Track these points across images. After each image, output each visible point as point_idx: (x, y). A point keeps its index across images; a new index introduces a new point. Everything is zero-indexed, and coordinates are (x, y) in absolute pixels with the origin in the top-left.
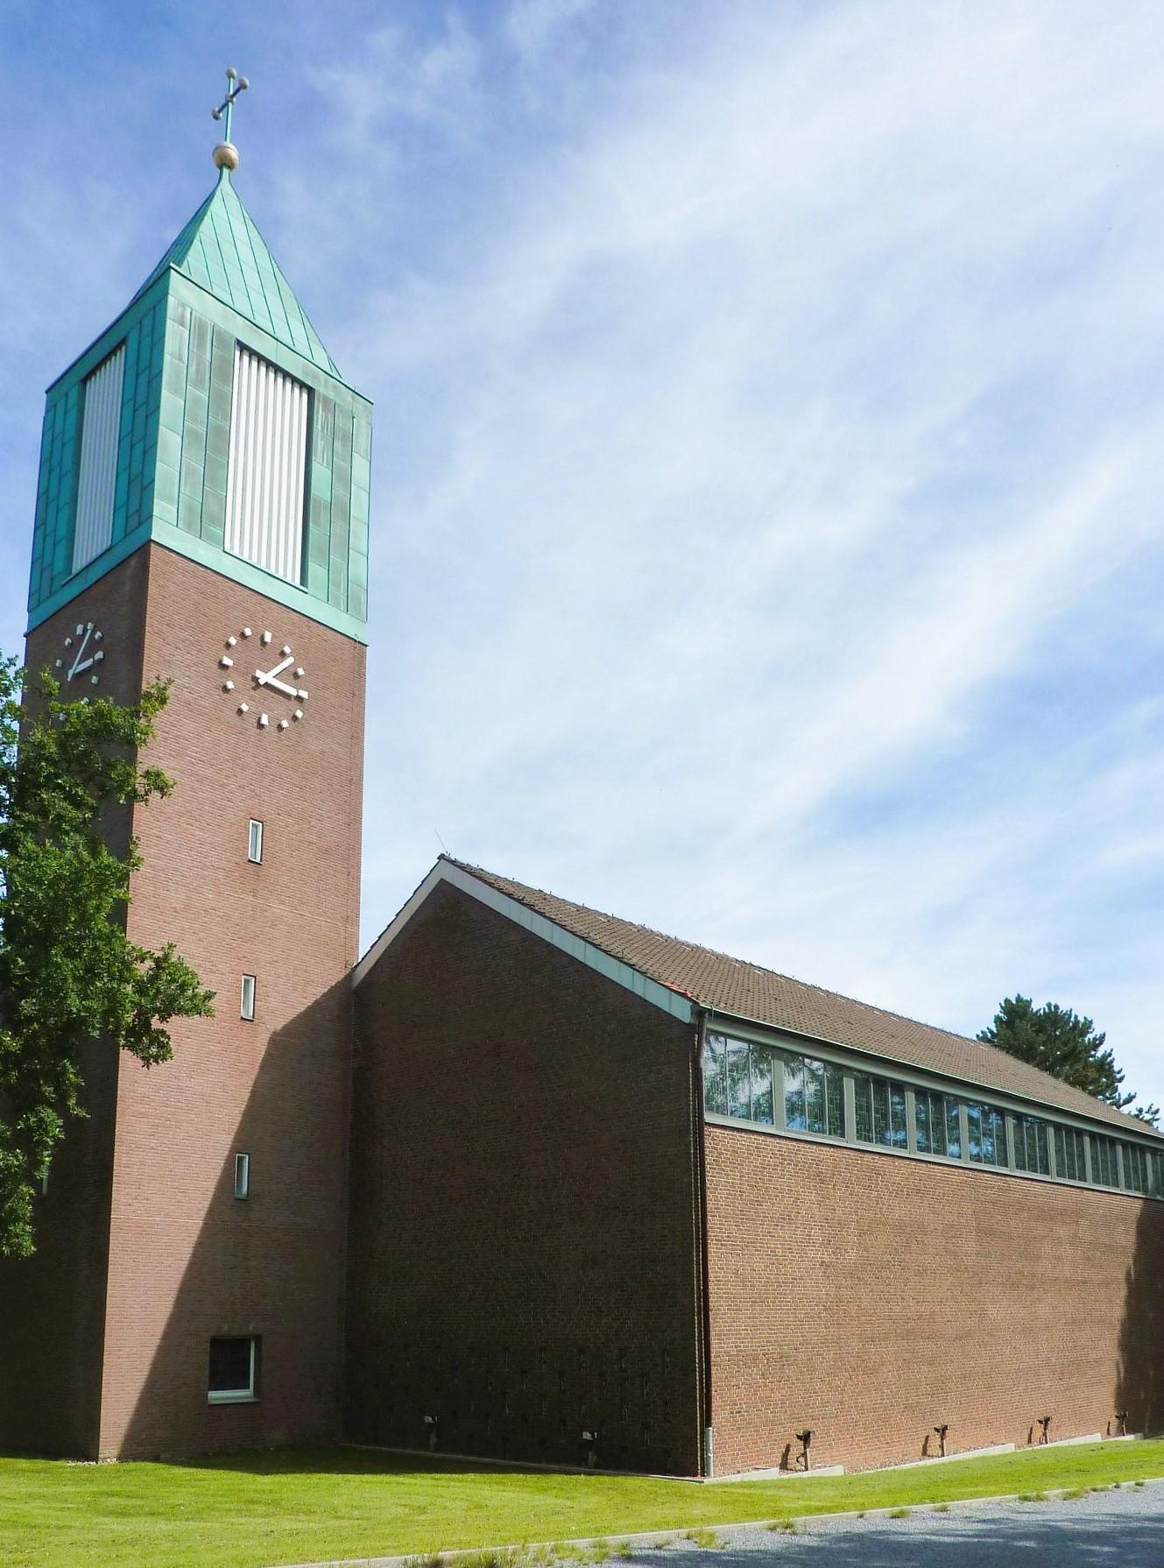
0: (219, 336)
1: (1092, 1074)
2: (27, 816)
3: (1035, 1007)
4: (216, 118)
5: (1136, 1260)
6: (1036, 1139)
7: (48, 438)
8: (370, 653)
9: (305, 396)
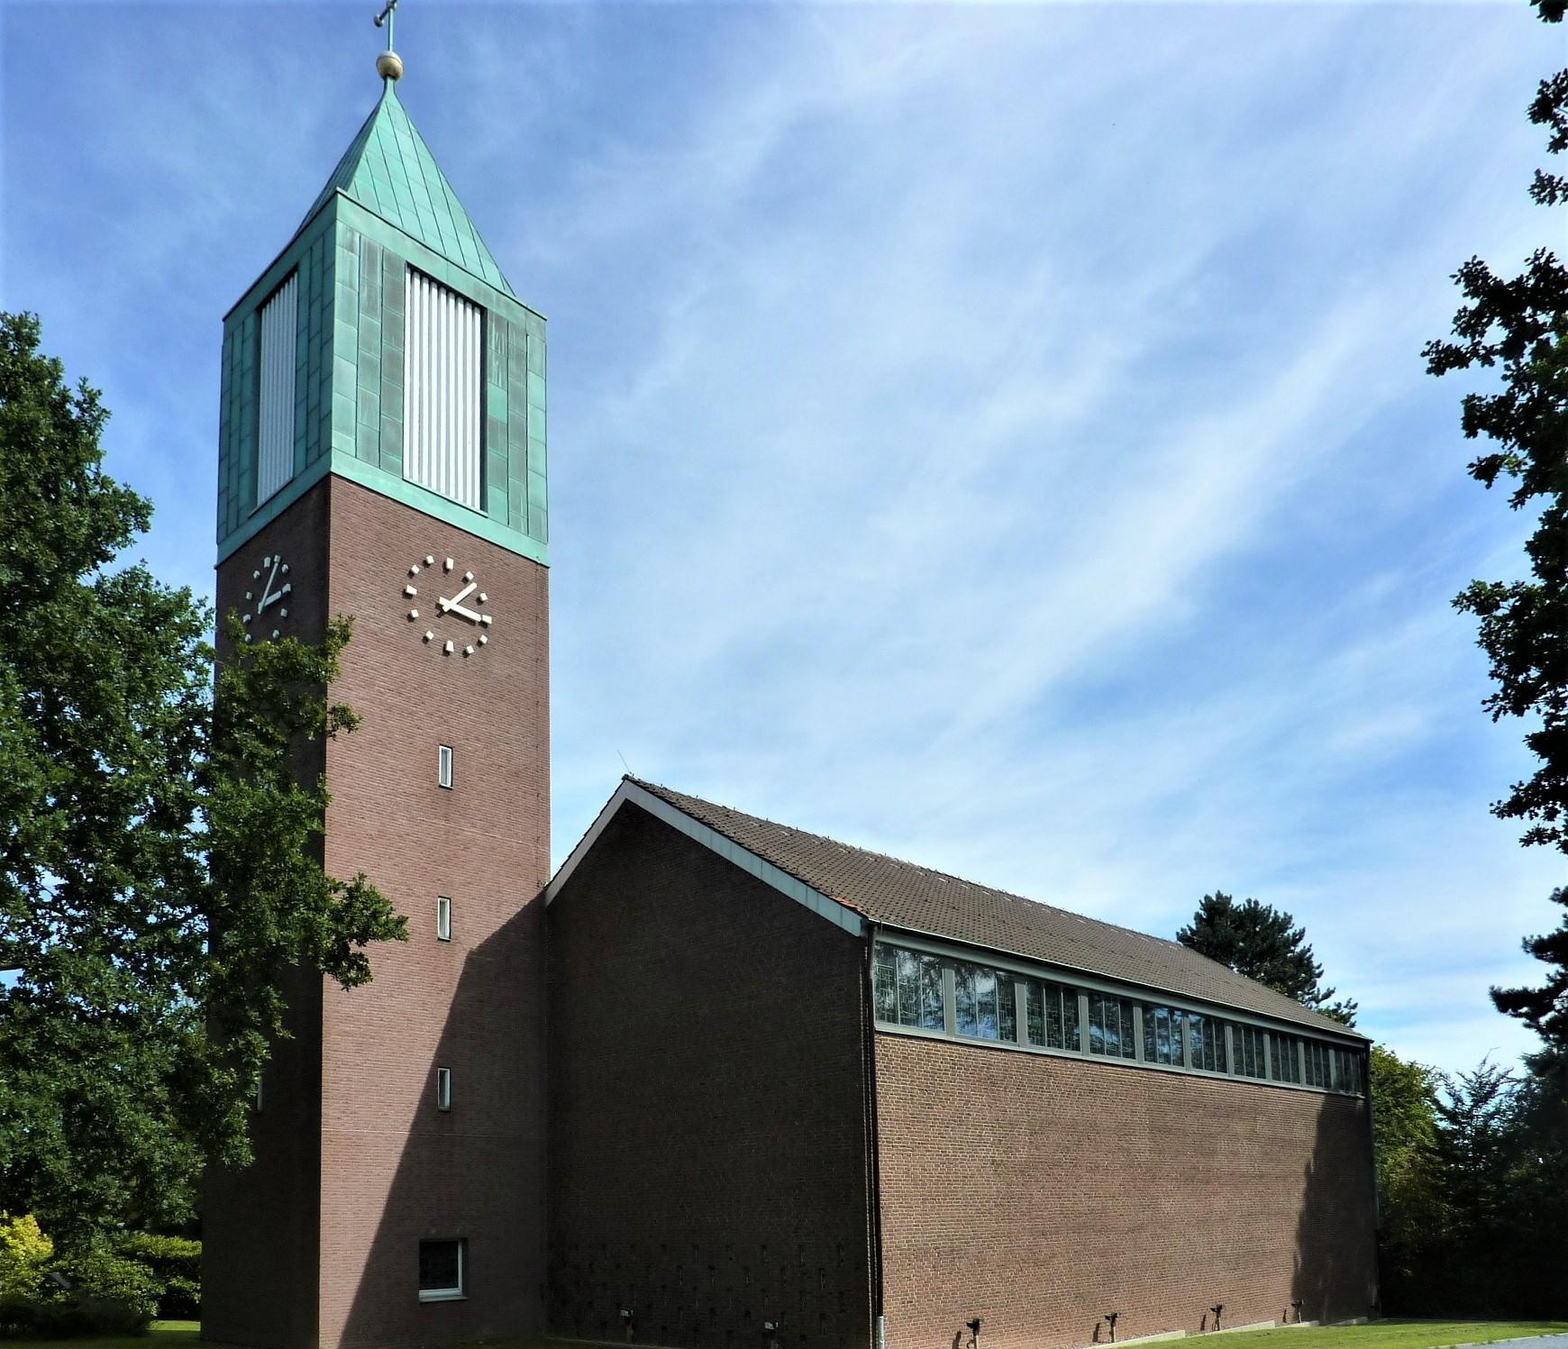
0: (389, 259)
1: (1290, 969)
2: (223, 756)
3: (1235, 903)
4: (378, 25)
5: (1317, 1153)
6: (1230, 1040)
7: (226, 435)
8: (552, 575)
9: (478, 316)
